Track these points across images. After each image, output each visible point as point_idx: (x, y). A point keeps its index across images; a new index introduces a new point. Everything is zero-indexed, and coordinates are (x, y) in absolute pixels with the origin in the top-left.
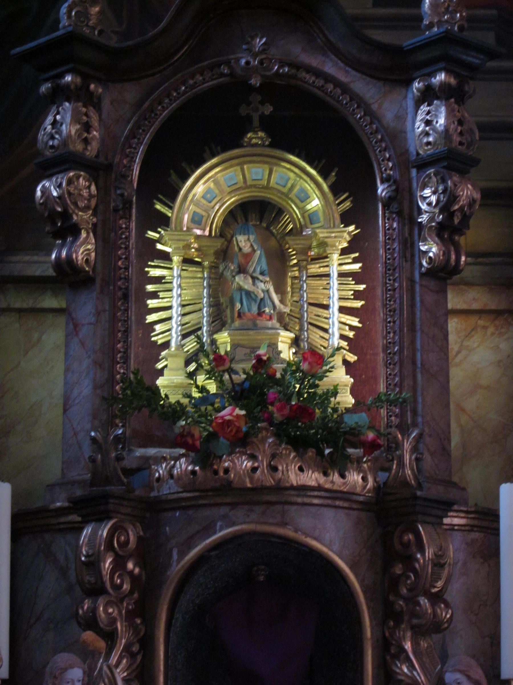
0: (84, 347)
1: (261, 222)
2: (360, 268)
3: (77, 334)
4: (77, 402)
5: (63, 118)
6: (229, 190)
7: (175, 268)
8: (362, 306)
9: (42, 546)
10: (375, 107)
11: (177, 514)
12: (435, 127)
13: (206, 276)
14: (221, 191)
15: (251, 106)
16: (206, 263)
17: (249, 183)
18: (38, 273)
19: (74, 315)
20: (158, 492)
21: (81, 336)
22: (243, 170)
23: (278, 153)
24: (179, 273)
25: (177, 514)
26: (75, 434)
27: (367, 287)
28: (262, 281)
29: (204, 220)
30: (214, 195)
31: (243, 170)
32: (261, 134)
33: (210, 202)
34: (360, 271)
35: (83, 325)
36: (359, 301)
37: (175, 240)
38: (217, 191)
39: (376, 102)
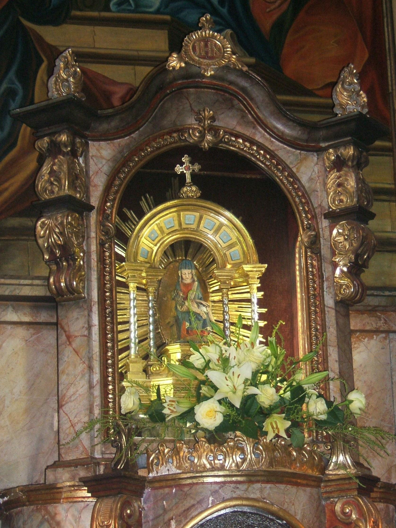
0: (78, 355)
1: (186, 256)
2: (262, 295)
3: (70, 344)
4: (73, 399)
5: (60, 168)
6: (167, 231)
7: (132, 292)
8: (265, 325)
9: (46, 517)
10: (294, 170)
11: (174, 491)
12: (347, 188)
13: (150, 298)
14: (162, 232)
15: (184, 166)
16: (151, 289)
17: (184, 226)
18: (7, 293)
19: (66, 328)
20: (157, 473)
21: (74, 345)
22: (179, 216)
23: (209, 204)
24: (135, 296)
25: (174, 491)
26: (72, 425)
27: (268, 310)
28: (204, 306)
29: (149, 255)
30: (157, 235)
31: (179, 216)
32: (194, 188)
33: (153, 241)
34: (262, 297)
35: (76, 337)
36: (263, 321)
37: (133, 270)
38: (159, 232)
39: (295, 167)
